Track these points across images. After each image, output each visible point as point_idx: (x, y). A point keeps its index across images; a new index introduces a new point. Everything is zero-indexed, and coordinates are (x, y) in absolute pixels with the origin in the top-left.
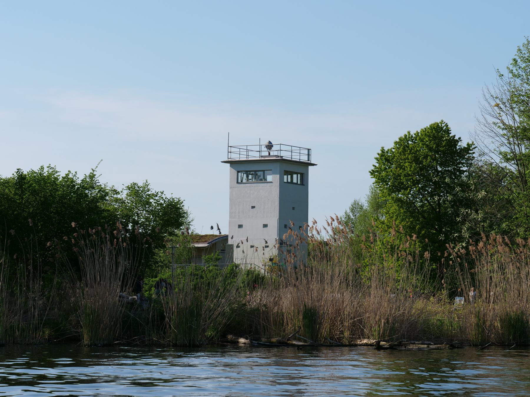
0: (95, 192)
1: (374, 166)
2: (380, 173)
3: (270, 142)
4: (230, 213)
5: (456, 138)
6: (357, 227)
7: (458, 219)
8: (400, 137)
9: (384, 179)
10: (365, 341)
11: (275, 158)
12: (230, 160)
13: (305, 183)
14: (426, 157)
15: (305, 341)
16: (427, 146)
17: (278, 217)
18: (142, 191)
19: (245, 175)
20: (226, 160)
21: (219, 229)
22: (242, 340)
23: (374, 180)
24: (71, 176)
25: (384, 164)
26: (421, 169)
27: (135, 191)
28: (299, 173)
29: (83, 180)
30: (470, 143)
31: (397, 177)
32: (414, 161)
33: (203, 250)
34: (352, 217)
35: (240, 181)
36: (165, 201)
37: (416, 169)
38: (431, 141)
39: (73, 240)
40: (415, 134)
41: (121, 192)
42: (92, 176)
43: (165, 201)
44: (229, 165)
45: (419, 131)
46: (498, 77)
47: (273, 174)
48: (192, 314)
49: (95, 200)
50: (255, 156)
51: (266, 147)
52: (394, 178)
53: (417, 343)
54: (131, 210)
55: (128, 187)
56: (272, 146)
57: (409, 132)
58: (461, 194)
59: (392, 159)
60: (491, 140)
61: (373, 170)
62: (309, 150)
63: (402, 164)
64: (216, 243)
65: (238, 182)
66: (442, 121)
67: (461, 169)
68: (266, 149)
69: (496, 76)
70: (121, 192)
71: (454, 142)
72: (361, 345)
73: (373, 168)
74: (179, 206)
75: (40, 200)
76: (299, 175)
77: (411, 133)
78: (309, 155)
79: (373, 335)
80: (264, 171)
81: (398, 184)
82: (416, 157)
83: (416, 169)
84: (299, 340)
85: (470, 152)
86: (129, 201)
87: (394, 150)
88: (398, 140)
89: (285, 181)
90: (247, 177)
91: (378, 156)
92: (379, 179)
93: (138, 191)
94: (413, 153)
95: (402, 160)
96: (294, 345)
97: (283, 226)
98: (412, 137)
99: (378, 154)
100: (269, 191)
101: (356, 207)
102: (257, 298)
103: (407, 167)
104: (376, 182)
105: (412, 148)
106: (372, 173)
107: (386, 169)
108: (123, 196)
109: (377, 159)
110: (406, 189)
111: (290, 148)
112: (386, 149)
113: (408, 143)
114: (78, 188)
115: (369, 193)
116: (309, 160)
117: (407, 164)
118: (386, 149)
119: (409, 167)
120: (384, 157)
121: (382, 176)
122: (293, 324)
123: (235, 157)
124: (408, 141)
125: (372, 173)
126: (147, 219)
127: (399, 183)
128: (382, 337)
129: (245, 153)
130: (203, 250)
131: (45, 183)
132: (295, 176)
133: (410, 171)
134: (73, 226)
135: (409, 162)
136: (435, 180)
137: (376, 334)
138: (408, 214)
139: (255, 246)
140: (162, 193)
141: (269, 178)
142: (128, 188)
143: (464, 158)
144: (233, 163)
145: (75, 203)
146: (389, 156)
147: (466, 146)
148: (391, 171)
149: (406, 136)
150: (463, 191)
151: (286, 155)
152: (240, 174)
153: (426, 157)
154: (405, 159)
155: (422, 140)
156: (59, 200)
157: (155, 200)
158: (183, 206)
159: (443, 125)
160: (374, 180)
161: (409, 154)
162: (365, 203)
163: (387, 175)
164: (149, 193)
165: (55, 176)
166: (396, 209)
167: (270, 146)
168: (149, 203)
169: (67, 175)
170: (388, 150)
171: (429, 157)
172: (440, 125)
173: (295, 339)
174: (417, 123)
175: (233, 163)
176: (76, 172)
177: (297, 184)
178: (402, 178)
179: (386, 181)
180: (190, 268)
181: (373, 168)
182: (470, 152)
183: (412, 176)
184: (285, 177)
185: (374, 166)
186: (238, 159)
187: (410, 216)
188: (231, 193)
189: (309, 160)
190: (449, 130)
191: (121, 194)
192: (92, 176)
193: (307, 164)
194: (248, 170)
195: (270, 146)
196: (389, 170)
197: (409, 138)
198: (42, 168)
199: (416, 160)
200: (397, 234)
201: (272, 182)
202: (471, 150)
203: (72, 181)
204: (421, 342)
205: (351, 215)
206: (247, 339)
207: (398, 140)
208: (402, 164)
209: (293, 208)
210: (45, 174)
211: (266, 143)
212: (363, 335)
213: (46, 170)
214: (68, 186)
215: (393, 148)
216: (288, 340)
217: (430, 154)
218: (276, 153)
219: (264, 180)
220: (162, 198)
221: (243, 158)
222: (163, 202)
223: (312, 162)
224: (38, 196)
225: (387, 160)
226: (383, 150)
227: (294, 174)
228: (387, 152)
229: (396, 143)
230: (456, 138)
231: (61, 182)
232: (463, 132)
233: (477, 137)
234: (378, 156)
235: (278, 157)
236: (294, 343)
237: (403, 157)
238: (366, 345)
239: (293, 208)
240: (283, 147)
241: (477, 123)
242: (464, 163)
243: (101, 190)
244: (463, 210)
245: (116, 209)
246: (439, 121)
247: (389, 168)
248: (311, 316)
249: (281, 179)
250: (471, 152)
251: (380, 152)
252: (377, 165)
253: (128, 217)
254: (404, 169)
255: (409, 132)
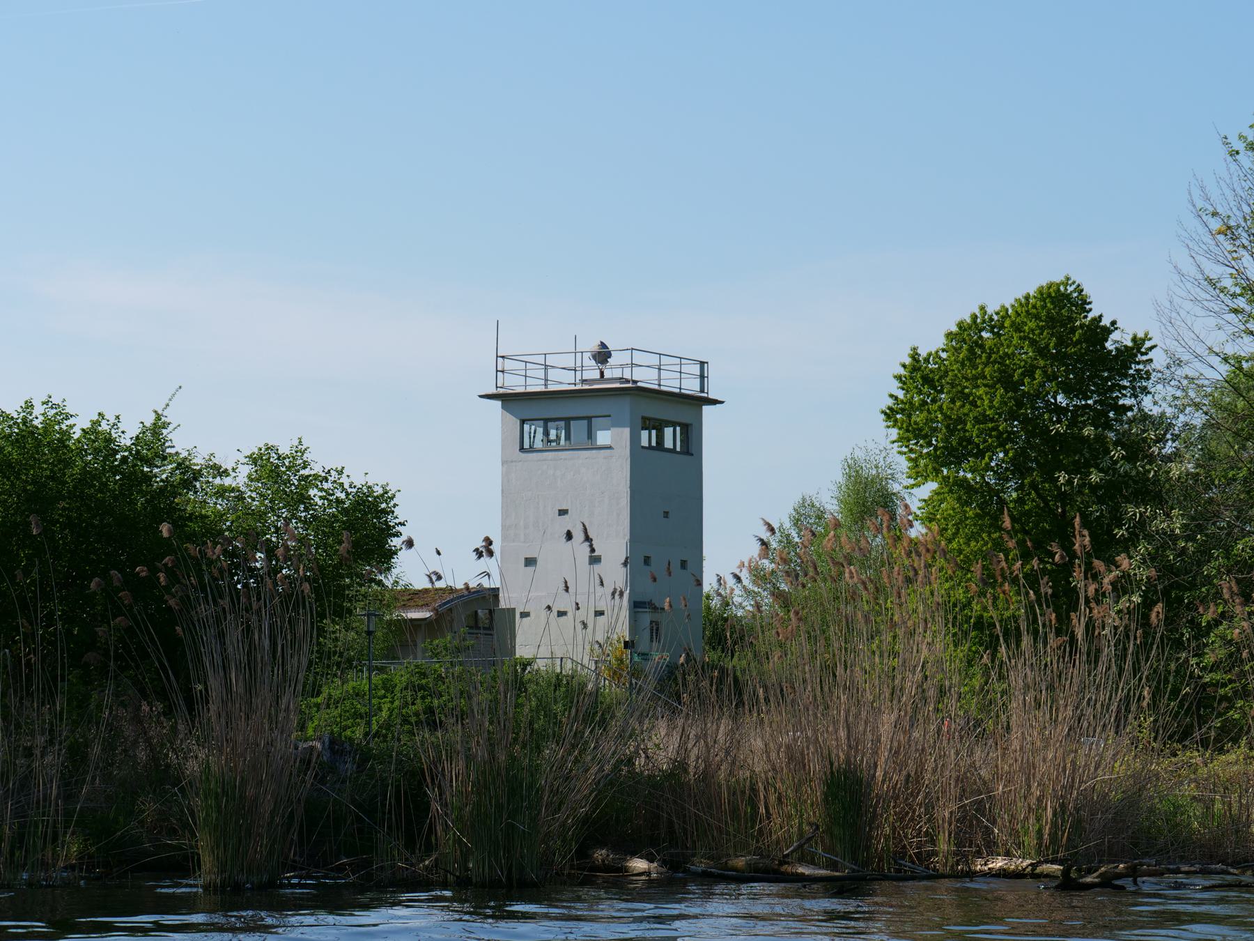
0: (163, 473)
1: (891, 396)
2: (909, 416)
3: (603, 345)
4: (503, 527)
5: (1106, 322)
6: (831, 558)
7: (1120, 533)
8: (958, 320)
9: (921, 430)
10: (999, 863)
11: (618, 385)
12: (501, 391)
13: (693, 450)
14: (1030, 372)
15: (833, 866)
16: (1033, 343)
17: (628, 537)
18: (289, 468)
19: (540, 430)
20: (493, 391)
21: (588, 539)
22: (639, 864)
23: (894, 433)
24: (104, 426)
25: (920, 393)
26: (1019, 404)
27: (273, 470)
28: (680, 424)
29: (137, 437)
30: (1141, 335)
31: (954, 425)
32: (999, 381)
33: (420, 626)
34: (797, 540)
35: (526, 446)
36: (348, 494)
37: (1006, 403)
38: (1042, 329)
39: (162, 576)
40: (997, 313)
41: (234, 470)
42: (159, 426)
43: (348, 494)
44: (498, 403)
45: (1008, 306)
46: (1229, 159)
47: (614, 425)
48: (508, 794)
49: (170, 490)
50: (563, 381)
51: (594, 357)
52: (948, 427)
53: (1185, 868)
54: (261, 516)
55: (250, 457)
56: (609, 355)
57: (982, 308)
58: (1123, 467)
59: (941, 378)
60: (1212, 321)
61: (890, 408)
62: (702, 363)
63: (967, 391)
64: (450, 610)
65: (522, 449)
66: (1068, 279)
67: (1121, 402)
68: (593, 363)
69: (1223, 152)
70: (234, 470)
71: (1099, 332)
72: (984, 874)
73: (890, 402)
74: (383, 506)
75: (25, 490)
76: (678, 429)
77: (990, 310)
78: (702, 377)
79: (1019, 845)
80: (589, 419)
81: (960, 444)
82: (1004, 372)
83: (1006, 403)
84: (812, 863)
85: (1140, 358)
86: (254, 495)
87: (944, 355)
88: (955, 329)
89: (645, 443)
90: (546, 433)
91: (902, 371)
92: (908, 431)
93: (277, 467)
94: (995, 362)
95: (967, 380)
96: (801, 878)
97: (640, 560)
98: (991, 319)
99: (904, 366)
100: (601, 473)
101: (807, 515)
102: (327, 744)
103: (980, 398)
104: (900, 439)
105: (990, 348)
106: (889, 414)
107: (924, 403)
108: (240, 478)
109: (899, 378)
110: (980, 454)
111: (654, 360)
112: (923, 353)
113: (981, 337)
114: (124, 459)
115: (840, 478)
116: (702, 391)
117: (981, 391)
118: (923, 353)
119: (988, 399)
120: (919, 374)
121: (916, 423)
122: (791, 818)
123: (515, 384)
124: (980, 331)
125: (889, 414)
126: (302, 541)
127: (961, 440)
128: (1045, 852)
129: (541, 374)
130: (420, 626)
131: (38, 444)
132: (668, 432)
133: (991, 408)
134: (165, 534)
135: (985, 386)
136: (1058, 431)
137: (1030, 841)
138: (987, 521)
139: (568, 622)
140: (340, 472)
141: (603, 437)
142: (254, 460)
143: (1125, 376)
144: (508, 399)
145: (115, 498)
146: (931, 371)
147: (1130, 344)
148: (941, 408)
149: (974, 317)
150: (1131, 458)
151: (646, 378)
152: (526, 427)
153: (1030, 372)
154: (975, 378)
155: (1017, 328)
156: (75, 487)
157: (322, 490)
158: (395, 505)
159: (1070, 289)
160: (894, 433)
161: (986, 365)
162: (831, 504)
163: (929, 421)
164: (306, 472)
165: (64, 427)
166: (954, 509)
167: (602, 355)
168: (304, 499)
169: (96, 423)
170: (930, 354)
171: (1038, 372)
172: (1062, 288)
173: (802, 860)
174: (1004, 285)
175: (508, 399)
176: (118, 417)
177: (673, 451)
178: (969, 426)
179: (925, 437)
180: (400, 673)
181: (890, 402)
182: (1140, 358)
183: (992, 420)
184: (645, 434)
185: (891, 396)
186: (521, 390)
187: (991, 525)
188: (506, 477)
189: (702, 391)
190: (1085, 302)
191: (233, 474)
192: (159, 426)
193: (701, 401)
194: (546, 414)
195: (602, 355)
196: (935, 407)
197: (984, 322)
198: (29, 405)
199: (1006, 380)
200: (959, 573)
201: (610, 448)
202: (1143, 354)
203: (109, 440)
204: (1197, 867)
205: (794, 534)
206: (651, 861)
207: (955, 329)
208: (967, 391)
209: (666, 514)
210: (36, 422)
211: (594, 346)
212: (991, 848)
213: (38, 410)
214: (97, 451)
215: (943, 350)
216: (782, 863)
217: (1042, 363)
218: (617, 373)
219: (589, 442)
220: (342, 485)
221: (536, 386)
222: (343, 496)
223: (711, 396)
224: (18, 478)
225: (927, 380)
226: (915, 356)
227: (667, 423)
228: (927, 360)
229: (949, 335)
230: (1106, 322)
231: (78, 441)
232: (1123, 306)
233: (1174, 315)
234: (902, 371)
235: (627, 381)
236: (801, 870)
237: (970, 373)
238: (1003, 874)
239: (666, 514)
240: (639, 358)
241: (1176, 278)
242: (1125, 388)
243: (183, 466)
244: (1131, 509)
245: (221, 516)
246: (1058, 278)
247: (934, 401)
248: (848, 794)
249: (635, 439)
250: (1145, 358)
251: (908, 361)
252: (901, 394)
253: (254, 539)
254: (974, 404)
255: (982, 308)
